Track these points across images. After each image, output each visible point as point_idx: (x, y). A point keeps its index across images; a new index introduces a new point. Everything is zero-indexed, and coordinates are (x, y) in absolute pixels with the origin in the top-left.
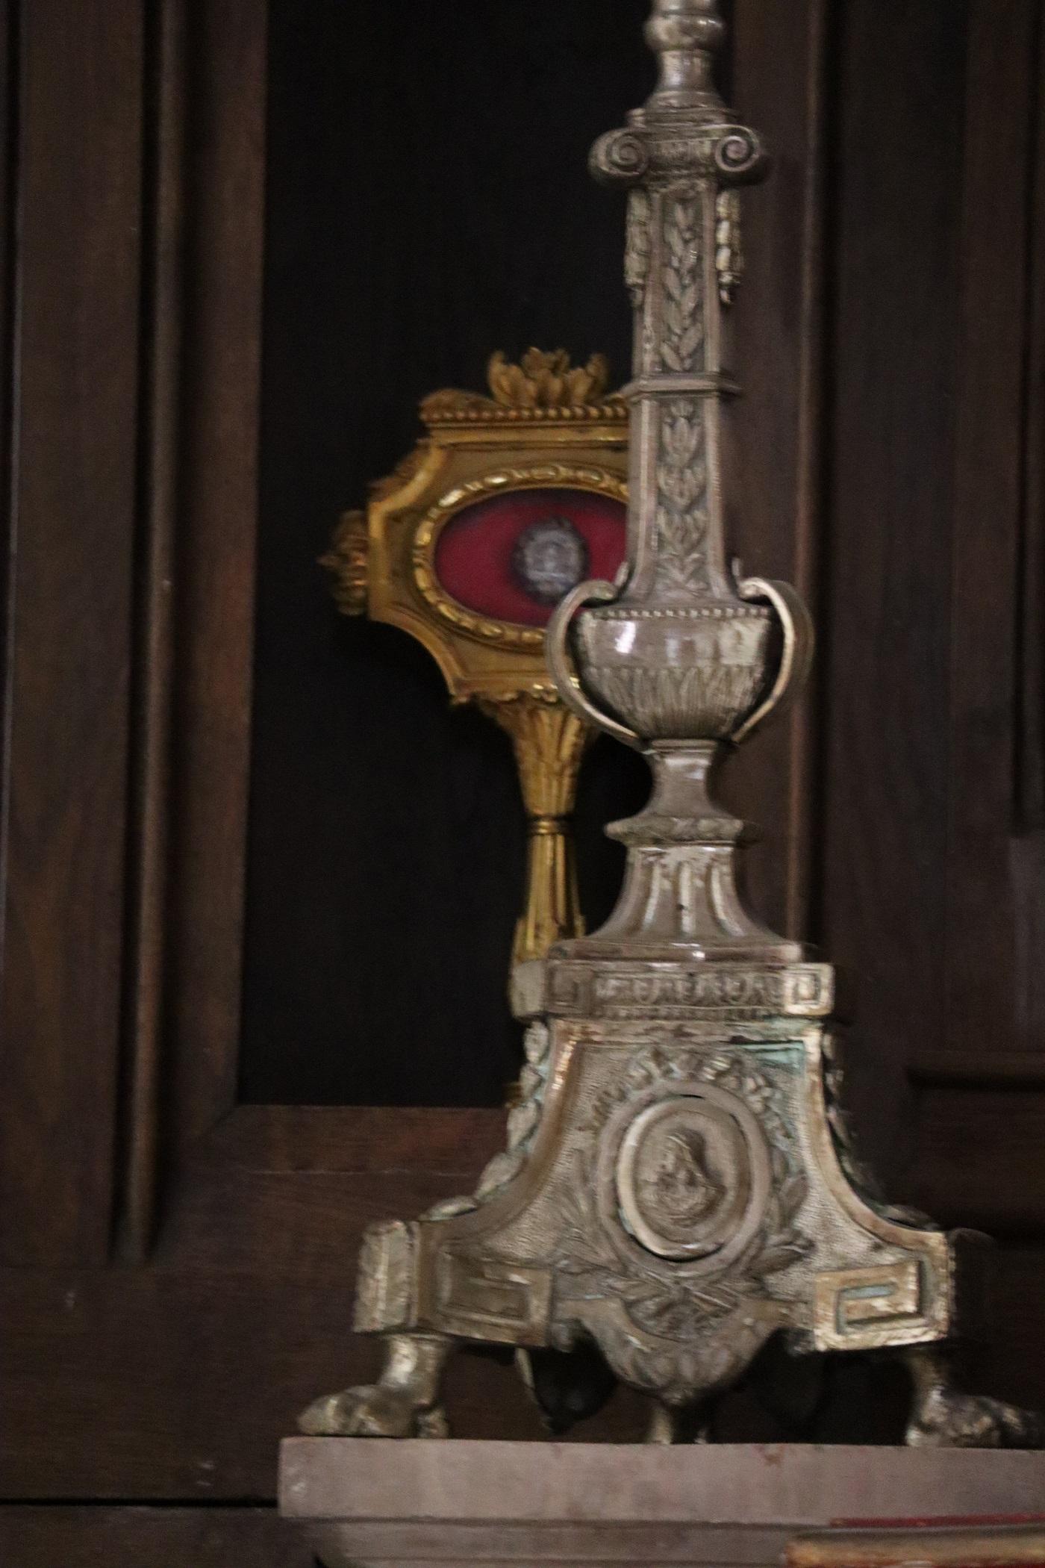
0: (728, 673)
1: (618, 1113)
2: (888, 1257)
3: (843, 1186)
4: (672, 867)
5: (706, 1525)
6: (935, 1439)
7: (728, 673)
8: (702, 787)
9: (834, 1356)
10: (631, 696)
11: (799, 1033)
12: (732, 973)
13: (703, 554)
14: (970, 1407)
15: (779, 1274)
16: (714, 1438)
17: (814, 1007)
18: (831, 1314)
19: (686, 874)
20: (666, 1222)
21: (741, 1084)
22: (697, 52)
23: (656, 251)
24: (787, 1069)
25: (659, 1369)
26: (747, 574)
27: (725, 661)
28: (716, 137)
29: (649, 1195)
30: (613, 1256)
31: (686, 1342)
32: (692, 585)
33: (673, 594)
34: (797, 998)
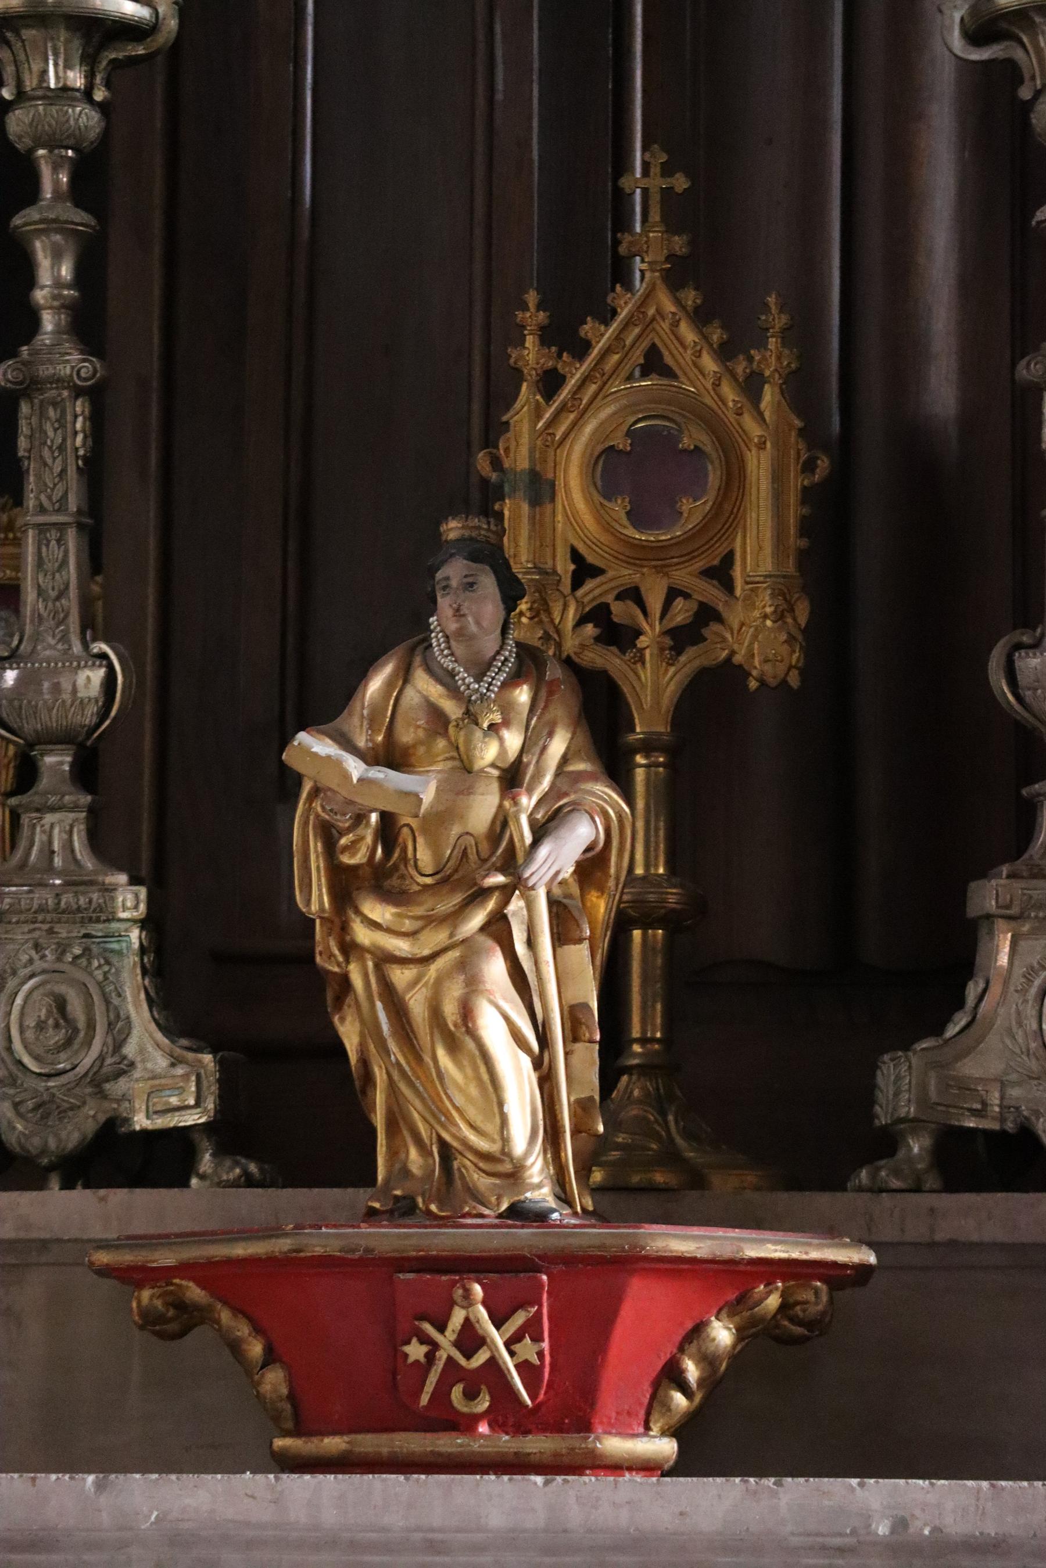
0: (82, 702)
1: (11, 984)
2: (180, 1071)
3: (153, 1026)
4: (47, 827)
5: (59, 1241)
6: (207, 1183)
7: (82, 702)
8: (67, 775)
9: (146, 1134)
10: (21, 719)
11: (126, 930)
12: (84, 893)
13: (68, 627)
14: (228, 1163)
15: (112, 1083)
16: (86, 1186)
17: (135, 914)
18: (144, 1107)
19: (56, 831)
20: (39, 1051)
21: (90, 963)
22: (63, 310)
23: (37, 435)
24: (120, 953)
25: (35, 1144)
26: (95, 639)
27: (79, 695)
28: (73, 363)
29: (30, 1034)
30: (6, 1073)
31: (51, 1126)
32: (60, 646)
33: (48, 653)
34: (125, 909)
